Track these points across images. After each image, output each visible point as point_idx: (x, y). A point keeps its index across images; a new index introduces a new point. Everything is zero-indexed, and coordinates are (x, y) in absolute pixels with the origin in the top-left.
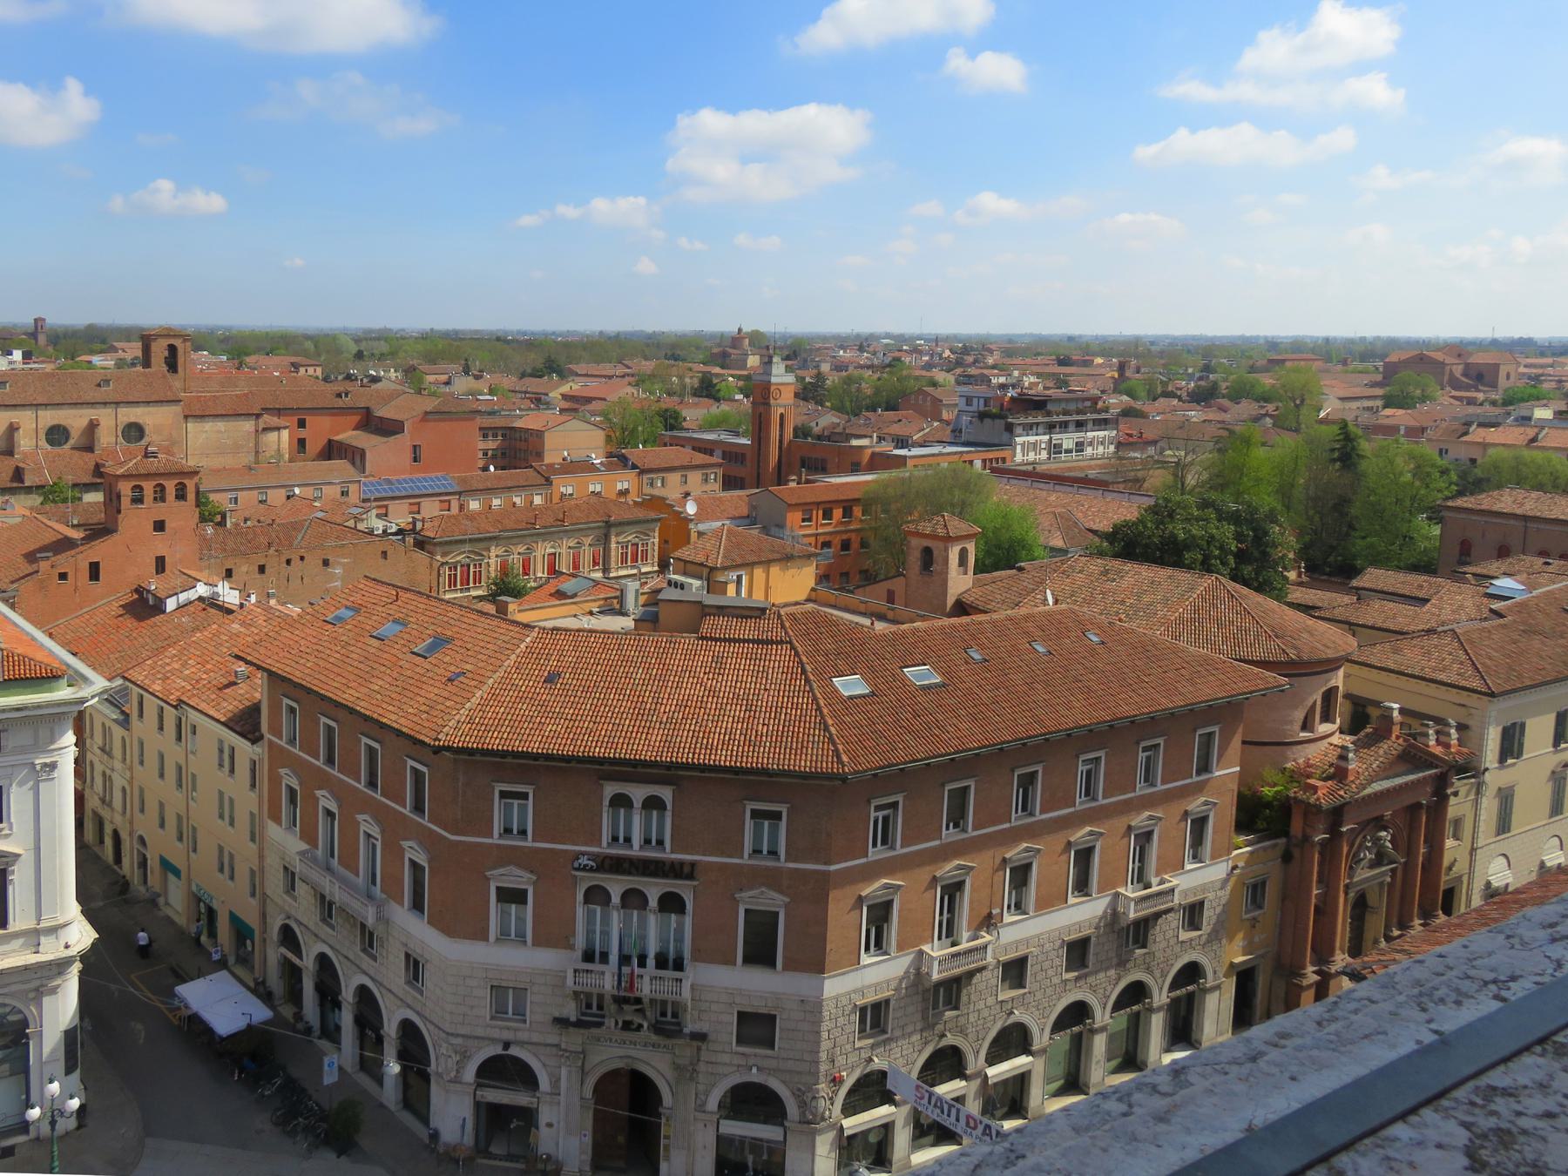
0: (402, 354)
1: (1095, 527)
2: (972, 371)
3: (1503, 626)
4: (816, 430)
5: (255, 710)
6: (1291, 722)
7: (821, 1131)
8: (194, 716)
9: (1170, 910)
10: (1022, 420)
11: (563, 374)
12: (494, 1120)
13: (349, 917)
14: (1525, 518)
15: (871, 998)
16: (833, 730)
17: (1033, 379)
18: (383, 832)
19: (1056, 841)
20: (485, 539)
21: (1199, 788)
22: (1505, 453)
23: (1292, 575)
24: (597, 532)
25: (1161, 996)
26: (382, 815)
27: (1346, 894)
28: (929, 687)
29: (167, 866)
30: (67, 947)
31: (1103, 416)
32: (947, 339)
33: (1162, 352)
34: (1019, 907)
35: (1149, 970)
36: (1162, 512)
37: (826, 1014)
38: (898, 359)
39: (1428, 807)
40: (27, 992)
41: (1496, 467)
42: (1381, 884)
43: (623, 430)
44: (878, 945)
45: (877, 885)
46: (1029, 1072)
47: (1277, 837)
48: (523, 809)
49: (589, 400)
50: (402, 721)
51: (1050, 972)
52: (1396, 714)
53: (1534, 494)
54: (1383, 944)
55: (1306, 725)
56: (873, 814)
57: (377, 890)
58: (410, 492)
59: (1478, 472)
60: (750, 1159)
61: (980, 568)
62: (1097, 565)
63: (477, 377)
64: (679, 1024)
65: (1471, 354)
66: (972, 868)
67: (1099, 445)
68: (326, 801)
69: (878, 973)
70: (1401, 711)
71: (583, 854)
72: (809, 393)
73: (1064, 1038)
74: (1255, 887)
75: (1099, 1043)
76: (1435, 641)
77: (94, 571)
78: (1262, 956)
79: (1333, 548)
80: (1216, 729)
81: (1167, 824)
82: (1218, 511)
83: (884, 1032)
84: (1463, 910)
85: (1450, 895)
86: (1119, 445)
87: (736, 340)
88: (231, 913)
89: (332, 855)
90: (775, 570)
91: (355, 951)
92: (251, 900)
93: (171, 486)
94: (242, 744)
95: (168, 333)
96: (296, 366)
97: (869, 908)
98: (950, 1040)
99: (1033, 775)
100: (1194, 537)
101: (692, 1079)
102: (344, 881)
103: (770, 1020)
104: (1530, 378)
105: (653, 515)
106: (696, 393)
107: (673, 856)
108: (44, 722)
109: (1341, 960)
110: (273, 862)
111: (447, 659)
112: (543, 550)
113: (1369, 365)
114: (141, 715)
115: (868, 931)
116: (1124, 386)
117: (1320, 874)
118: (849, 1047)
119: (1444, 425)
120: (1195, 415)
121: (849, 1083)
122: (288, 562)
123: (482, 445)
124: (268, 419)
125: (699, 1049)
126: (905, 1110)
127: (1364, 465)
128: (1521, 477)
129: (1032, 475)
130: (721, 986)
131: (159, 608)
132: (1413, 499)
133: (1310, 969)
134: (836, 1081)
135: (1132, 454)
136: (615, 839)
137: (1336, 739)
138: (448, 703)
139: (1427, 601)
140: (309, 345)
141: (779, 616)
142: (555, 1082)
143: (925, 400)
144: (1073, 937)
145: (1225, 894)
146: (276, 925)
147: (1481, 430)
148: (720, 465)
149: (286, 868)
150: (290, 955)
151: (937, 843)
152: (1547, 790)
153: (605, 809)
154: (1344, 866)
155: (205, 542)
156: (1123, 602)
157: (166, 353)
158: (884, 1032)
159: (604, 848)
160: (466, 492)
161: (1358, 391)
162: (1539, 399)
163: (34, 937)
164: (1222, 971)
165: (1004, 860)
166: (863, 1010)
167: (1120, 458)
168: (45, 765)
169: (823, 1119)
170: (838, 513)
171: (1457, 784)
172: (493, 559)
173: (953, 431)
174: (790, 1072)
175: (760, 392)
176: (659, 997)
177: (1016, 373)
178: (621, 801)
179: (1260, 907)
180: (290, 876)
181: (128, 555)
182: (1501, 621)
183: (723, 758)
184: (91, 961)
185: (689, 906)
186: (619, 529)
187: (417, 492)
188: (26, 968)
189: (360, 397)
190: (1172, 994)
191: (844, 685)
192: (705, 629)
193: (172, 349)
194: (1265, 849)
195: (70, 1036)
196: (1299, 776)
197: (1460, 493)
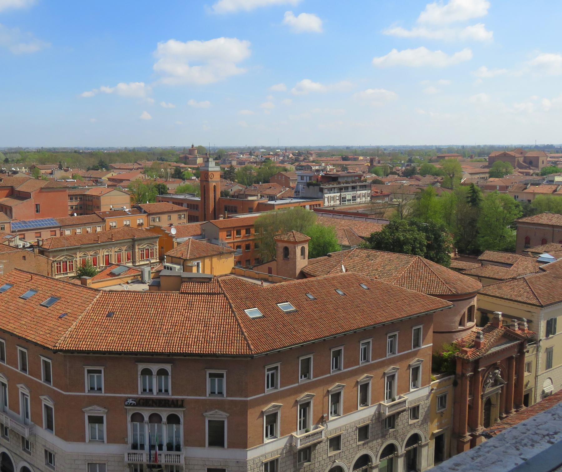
0: (27, 160)
1: (363, 235)
2: (303, 164)
3: (545, 275)
4: (231, 193)
6: (455, 322)
9: (320, 442)
10: (327, 186)
11: (108, 169)
14: (553, 226)
15: (270, 459)
16: (246, 334)
17: (331, 167)
18: (30, 392)
19: (351, 382)
20: (74, 249)
21: (415, 354)
23: (452, 255)
25: (402, 450)
26: (29, 384)
27: (482, 399)
28: (290, 312)
31: (364, 184)
32: (291, 149)
33: (389, 154)
34: (336, 413)
35: (396, 438)
36: (393, 228)
37: (249, 467)
38: (268, 159)
39: (516, 358)
42: (497, 394)
43: (139, 195)
44: (272, 433)
45: (270, 406)
48: (99, 378)
49: (121, 181)
50: (37, 338)
51: (352, 442)
52: (500, 316)
53: (556, 215)
54: (499, 421)
56: (266, 373)
57: (29, 420)
58: (36, 227)
59: (532, 206)
61: (311, 256)
63: (66, 171)
65: (526, 152)
66: (313, 396)
67: (362, 197)
70: (503, 315)
71: (130, 398)
72: (227, 175)
74: (441, 398)
78: (446, 429)
79: (469, 242)
80: (421, 326)
82: (418, 226)
84: (533, 404)
85: (527, 397)
86: (372, 197)
87: (191, 151)
90: (215, 260)
100: (407, 239)
102: (12, 417)
104: (552, 163)
105: (155, 235)
106: (173, 176)
107: (173, 397)
109: (481, 429)
112: (103, 253)
113: (482, 158)
115: (267, 428)
119: (516, 185)
120: (406, 182)
127: (482, 204)
128: (550, 208)
129: (332, 212)
132: (504, 219)
137: (475, 329)
138: (60, 329)
139: (512, 265)
141: (218, 282)
143: (281, 178)
145: (428, 402)
147: (532, 187)
148: (186, 211)
151: (297, 385)
153: (139, 376)
156: (377, 270)
159: (140, 395)
160: (62, 227)
161: (477, 170)
166: (266, 464)
170: (243, 232)
171: (528, 347)
172: (78, 258)
173: (295, 192)
175: (204, 175)
176: (169, 464)
177: (323, 164)
178: (147, 372)
179: (444, 407)
183: (195, 350)
185: (182, 420)
186: (139, 242)
187: (39, 227)
191: (250, 313)
194: (445, 380)
196: (459, 347)
197: (524, 216)
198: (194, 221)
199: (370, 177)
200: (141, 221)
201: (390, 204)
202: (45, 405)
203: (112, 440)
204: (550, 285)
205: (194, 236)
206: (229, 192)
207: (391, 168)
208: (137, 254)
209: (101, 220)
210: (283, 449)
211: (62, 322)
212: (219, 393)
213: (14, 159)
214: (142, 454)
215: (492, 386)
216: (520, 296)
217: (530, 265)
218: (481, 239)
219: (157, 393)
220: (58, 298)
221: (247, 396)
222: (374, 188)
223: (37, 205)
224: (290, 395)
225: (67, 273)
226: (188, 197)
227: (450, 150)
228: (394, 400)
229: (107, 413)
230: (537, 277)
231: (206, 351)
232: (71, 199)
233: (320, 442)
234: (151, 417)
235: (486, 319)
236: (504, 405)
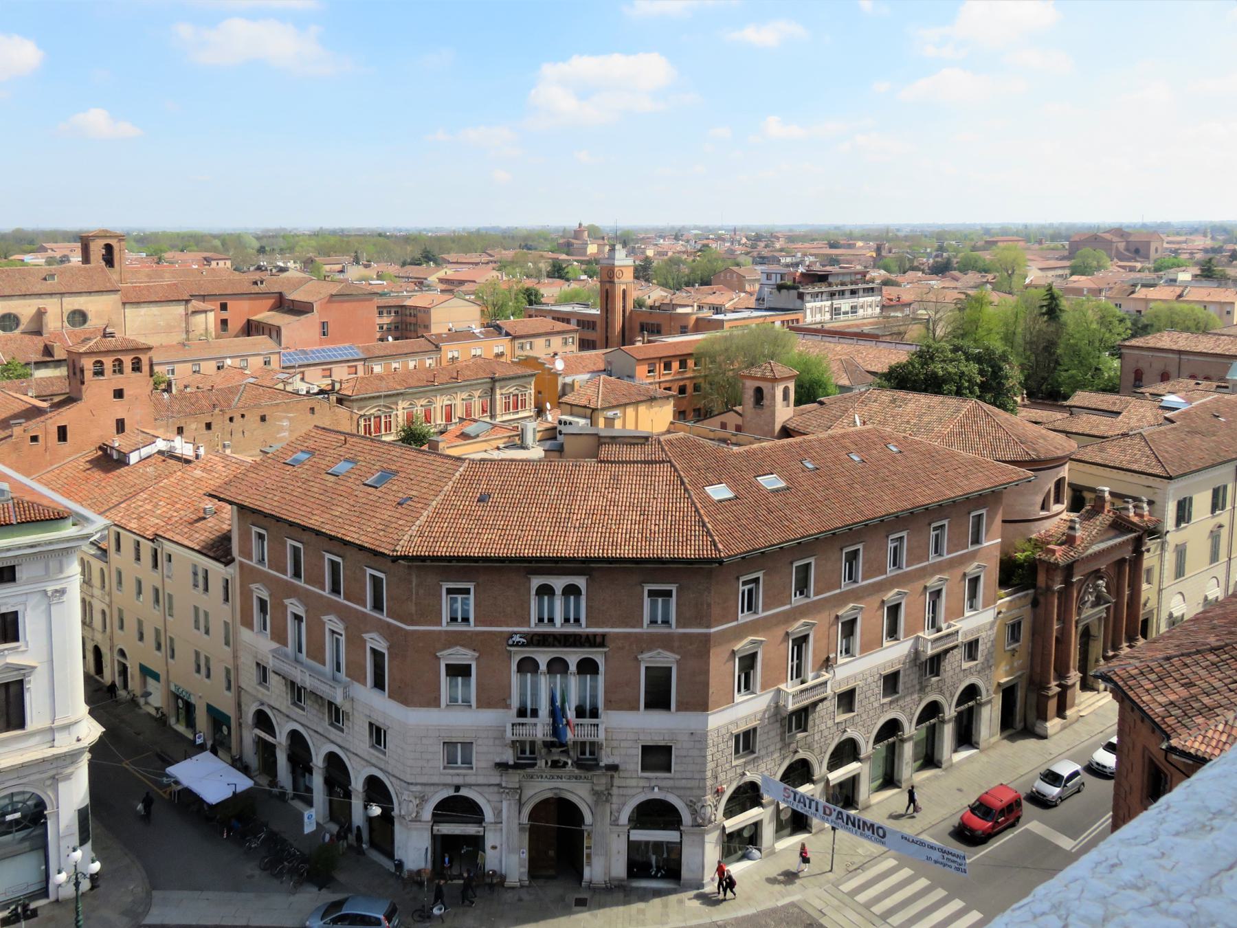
0: (297, 249)
1: (873, 369)
2: (765, 253)
3: (1174, 429)
4: (649, 302)
5: (226, 539)
6: (1033, 505)
7: (709, 832)
8: (169, 547)
9: (956, 647)
10: (810, 290)
12: (444, 846)
13: (317, 697)
14: (1180, 352)
15: (743, 727)
17: (812, 259)
18: (346, 629)
19: (874, 601)
21: (972, 556)
22: (1163, 306)
23: (1018, 399)
25: (950, 712)
26: (344, 614)
28: (777, 490)
29: (145, 672)
30: (79, 740)
31: (871, 285)
33: (906, 236)
35: (941, 692)
36: (925, 356)
37: (710, 742)
38: (707, 246)
40: (44, 780)
41: (1156, 316)
42: (1100, 619)
44: (747, 687)
46: (859, 774)
48: (465, 603)
49: (462, 283)
50: (363, 538)
51: (872, 699)
52: (1107, 494)
53: (1185, 335)
54: (1102, 662)
56: (741, 588)
57: (342, 675)
58: (323, 360)
59: (1144, 320)
60: (653, 858)
61: (798, 402)
62: (887, 396)
63: (366, 266)
64: (596, 760)
66: (814, 624)
67: (867, 309)
69: (746, 709)
70: (1111, 493)
71: (516, 633)
72: (643, 272)
73: (881, 746)
74: (1013, 626)
75: (908, 750)
77: (62, 433)
78: (1019, 677)
79: (1045, 379)
80: (984, 511)
81: (952, 586)
82: (965, 353)
83: (896, 692)
85: (1145, 623)
86: (883, 307)
87: (578, 233)
88: (209, 706)
90: (642, 409)
91: (323, 725)
92: (227, 693)
93: (127, 361)
94: (215, 567)
95: (104, 234)
96: (208, 260)
97: (793, 641)
98: (801, 755)
99: (856, 552)
100: (949, 373)
101: (607, 801)
102: (314, 673)
103: (667, 750)
104: (1171, 251)
105: (529, 372)
106: (550, 275)
108: (62, 552)
109: (1074, 676)
111: (395, 488)
112: (441, 402)
113: (1058, 244)
114: (118, 548)
116: (881, 263)
118: (727, 766)
119: (1118, 286)
120: (936, 283)
121: (729, 792)
122: (231, 419)
123: (379, 321)
124: (195, 304)
125: (612, 777)
126: (770, 810)
127: (1064, 317)
128: (1174, 323)
130: (627, 728)
131: (122, 461)
132: (1101, 341)
133: (1053, 683)
134: (719, 792)
137: (1065, 516)
138: (401, 522)
139: (1120, 413)
140: (217, 243)
141: (659, 442)
142: (498, 813)
143: (732, 277)
146: (250, 711)
147: (1144, 289)
148: (576, 331)
149: (258, 664)
150: (263, 735)
151: (788, 607)
152: (1207, 545)
154: (1071, 609)
155: (157, 405)
156: (908, 422)
157: (104, 251)
158: (753, 752)
159: (533, 627)
161: (1052, 263)
163: (51, 732)
164: (993, 688)
166: (737, 737)
167: (884, 317)
168: (56, 591)
169: (710, 822)
170: (675, 365)
173: (758, 300)
174: (684, 788)
175: (608, 276)
176: (580, 739)
178: (545, 591)
179: (1017, 641)
180: (263, 671)
181: (92, 419)
183: (627, 552)
184: (97, 749)
185: (602, 668)
186: (502, 383)
187: (329, 360)
188: (44, 760)
189: (273, 284)
190: (959, 709)
192: (602, 456)
193: (109, 248)
194: (1019, 598)
195: (83, 815)
196: (1040, 544)
197: (1133, 336)
199: (878, 274)
200: (501, 349)
201: (914, 319)
202: (372, 649)
203: (485, 702)
204: (1181, 444)
205: (593, 372)
206: (644, 301)
207: (911, 261)
208: (498, 403)
210: (764, 713)
211: (405, 512)
212: (663, 622)
214: (535, 725)
215: (1093, 606)
216: (1136, 461)
217: (1149, 414)
221: (709, 627)
224: (777, 624)
227: (1005, 231)
228: (939, 630)
229: (477, 659)
230: (1160, 432)
231: (646, 553)
232: (380, 313)
234: (550, 664)
236: (1110, 637)
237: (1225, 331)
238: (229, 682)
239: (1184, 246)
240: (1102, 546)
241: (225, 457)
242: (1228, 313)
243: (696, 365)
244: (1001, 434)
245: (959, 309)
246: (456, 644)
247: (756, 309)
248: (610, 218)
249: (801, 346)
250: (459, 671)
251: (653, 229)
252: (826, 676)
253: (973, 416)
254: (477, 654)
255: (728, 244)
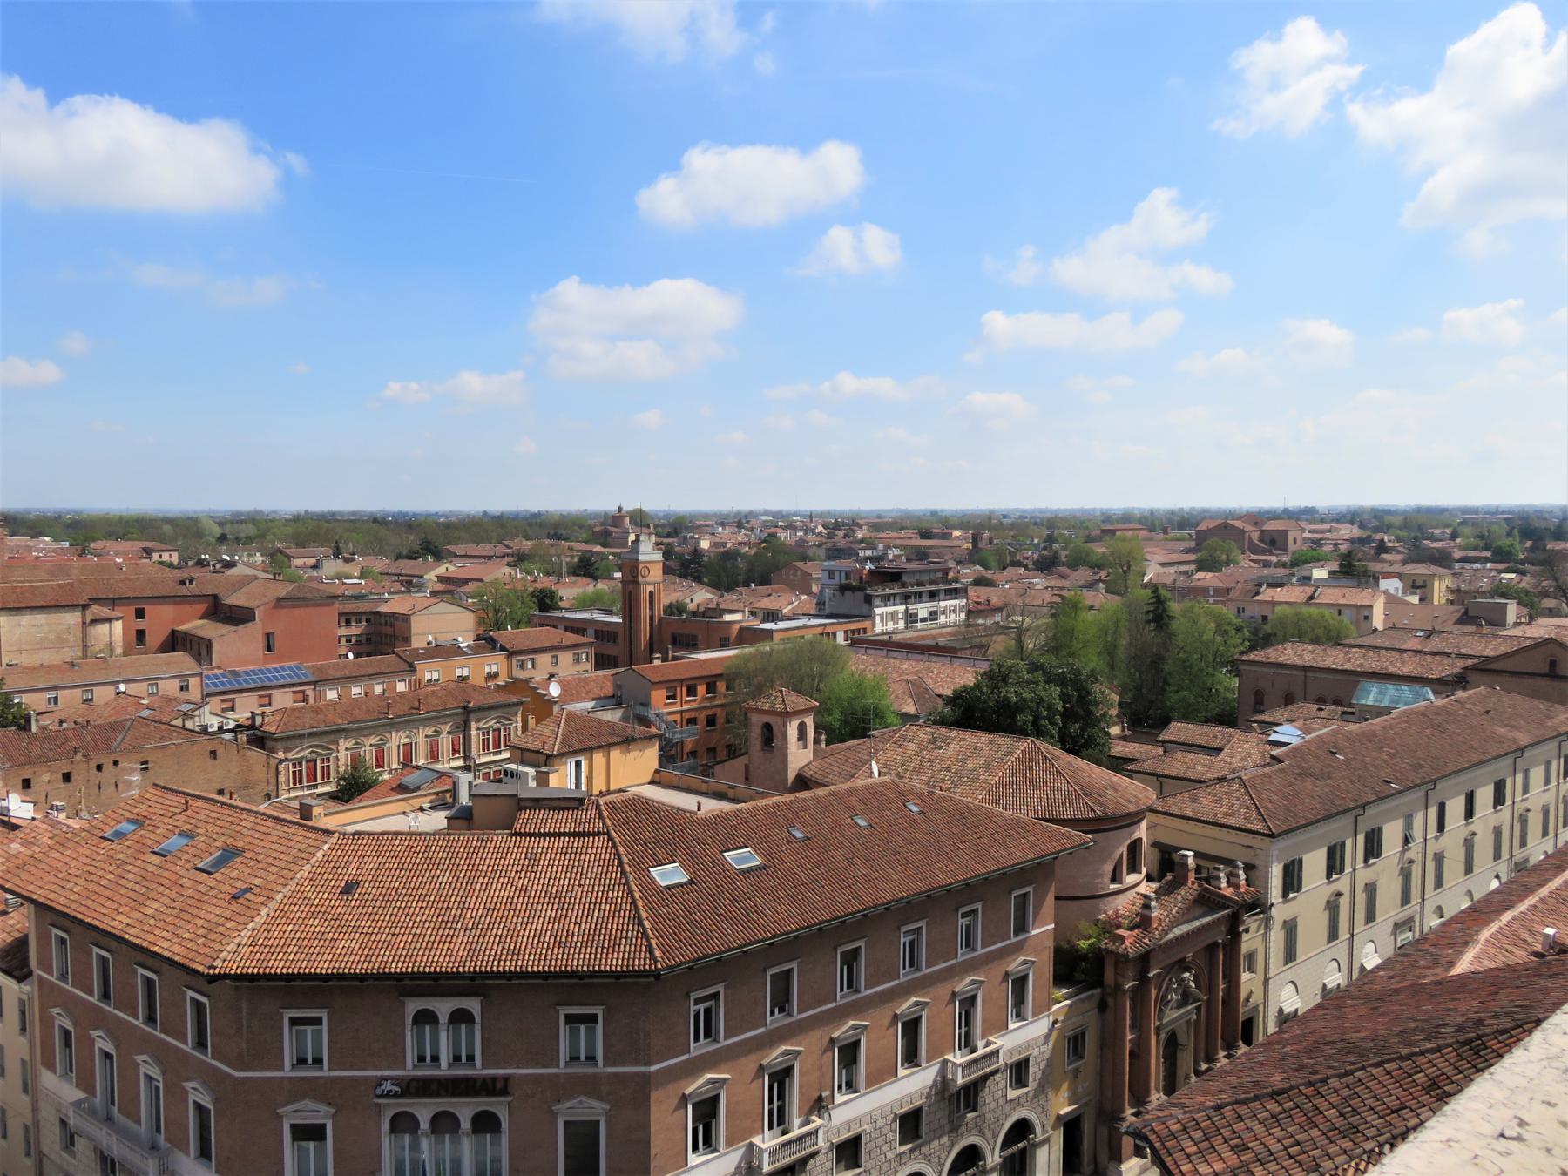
3: (1281, 770)
4: (692, 607)
5: (21, 944)
6: (1101, 876)
9: (814, 1155)
10: (880, 592)
11: (439, 556)
14: (1305, 669)
16: (647, 924)
17: (897, 552)
18: (164, 1073)
19: (883, 1015)
20: (332, 732)
21: (1017, 948)
22: (1288, 610)
24: (456, 719)
26: (162, 1055)
27: (1158, 1035)
28: (749, 870)
31: (954, 586)
32: (821, 515)
34: (850, 1086)
35: (981, 1133)
36: (996, 677)
38: (773, 535)
39: (1224, 946)
42: (1189, 1022)
44: (707, 1142)
45: (701, 1081)
47: (1093, 987)
49: (465, 581)
50: (176, 948)
54: (1193, 1078)
55: (1115, 878)
56: (693, 1008)
58: (260, 684)
59: (1268, 628)
62: (924, 734)
63: (347, 560)
65: (1264, 523)
66: (799, 1052)
67: (951, 613)
68: (103, 1043)
70: (1197, 855)
74: (1075, 1038)
76: (1225, 789)
78: (1086, 1104)
80: (1030, 889)
83: (918, 1136)
84: (1261, 1039)
85: (1249, 1024)
86: (969, 613)
87: (617, 519)
89: (113, 1103)
90: (615, 754)
96: (148, 552)
97: (694, 1105)
100: (1024, 699)
102: (124, 1134)
105: (514, 699)
107: (486, 1072)
110: (48, 1116)
111: (234, 874)
112: (397, 740)
115: (695, 1131)
117: (1132, 1019)
119: (1241, 586)
122: (99, 768)
123: (343, 631)
124: (96, 610)
127: (1174, 625)
128: (1302, 631)
129: (889, 645)
135: (981, 621)
136: (422, 1059)
141: (598, 806)
144: (906, 1109)
145: (1047, 1049)
148: (591, 644)
151: (762, 1030)
152: (1323, 919)
153: (408, 1028)
156: (948, 769)
159: (410, 1070)
160: (319, 683)
161: (1175, 557)
162: (1317, 560)
165: (832, 1040)
170: (702, 689)
171: (1248, 921)
172: (342, 753)
175: (632, 571)
177: (881, 547)
178: (425, 1018)
179: (1082, 1057)
182: (1280, 766)
183: (531, 963)
185: (505, 1124)
186: (480, 715)
187: (267, 683)
189: (206, 582)
191: (662, 875)
194: (1082, 1001)
196: (1108, 928)
197: (1253, 648)
198: (609, 667)
200: (495, 668)
202: (195, 1102)
204: (1288, 790)
205: (598, 699)
207: (1013, 554)
208: (474, 740)
209: (406, 667)
211: (238, 909)
212: (587, 1058)
213: (243, 535)
215: (1178, 1007)
216: (1233, 815)
218: (1176, 697)
219: (450, 1065)
220: (239, 852)
221: (647, 1064)
222: (976, 593)
223: (268, 635)
224: (750, 1052)
225: (316, 786)
226: (598, 616)
227: (1127, 518)
228: (974, 1050)
229: (334, 1116)
232: (348, 622)
233: (814, 1155)
235: (1168, 866)
236: (1202, 1045)
237: (1360, 641)
238: (28, 1143)
239: (1328, 535)
240: (1185, 928)
241: (55, 824)
242: (1366, 618)
243: (728, 688)
244: (1060, 784)
245: (1053, 615)
246: (304, 1098)
247: (815, 616)
248: (662, 501)
249: (862, 665)
250: (308, 1133)
251: (715, 515)
252: (817, 1121)
253: (1027, 761)
254: (332, 1110)
255: (800, 534)
